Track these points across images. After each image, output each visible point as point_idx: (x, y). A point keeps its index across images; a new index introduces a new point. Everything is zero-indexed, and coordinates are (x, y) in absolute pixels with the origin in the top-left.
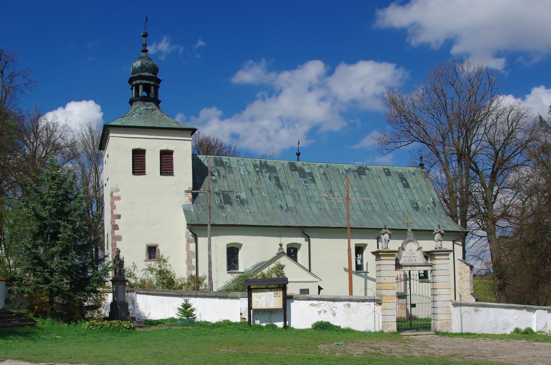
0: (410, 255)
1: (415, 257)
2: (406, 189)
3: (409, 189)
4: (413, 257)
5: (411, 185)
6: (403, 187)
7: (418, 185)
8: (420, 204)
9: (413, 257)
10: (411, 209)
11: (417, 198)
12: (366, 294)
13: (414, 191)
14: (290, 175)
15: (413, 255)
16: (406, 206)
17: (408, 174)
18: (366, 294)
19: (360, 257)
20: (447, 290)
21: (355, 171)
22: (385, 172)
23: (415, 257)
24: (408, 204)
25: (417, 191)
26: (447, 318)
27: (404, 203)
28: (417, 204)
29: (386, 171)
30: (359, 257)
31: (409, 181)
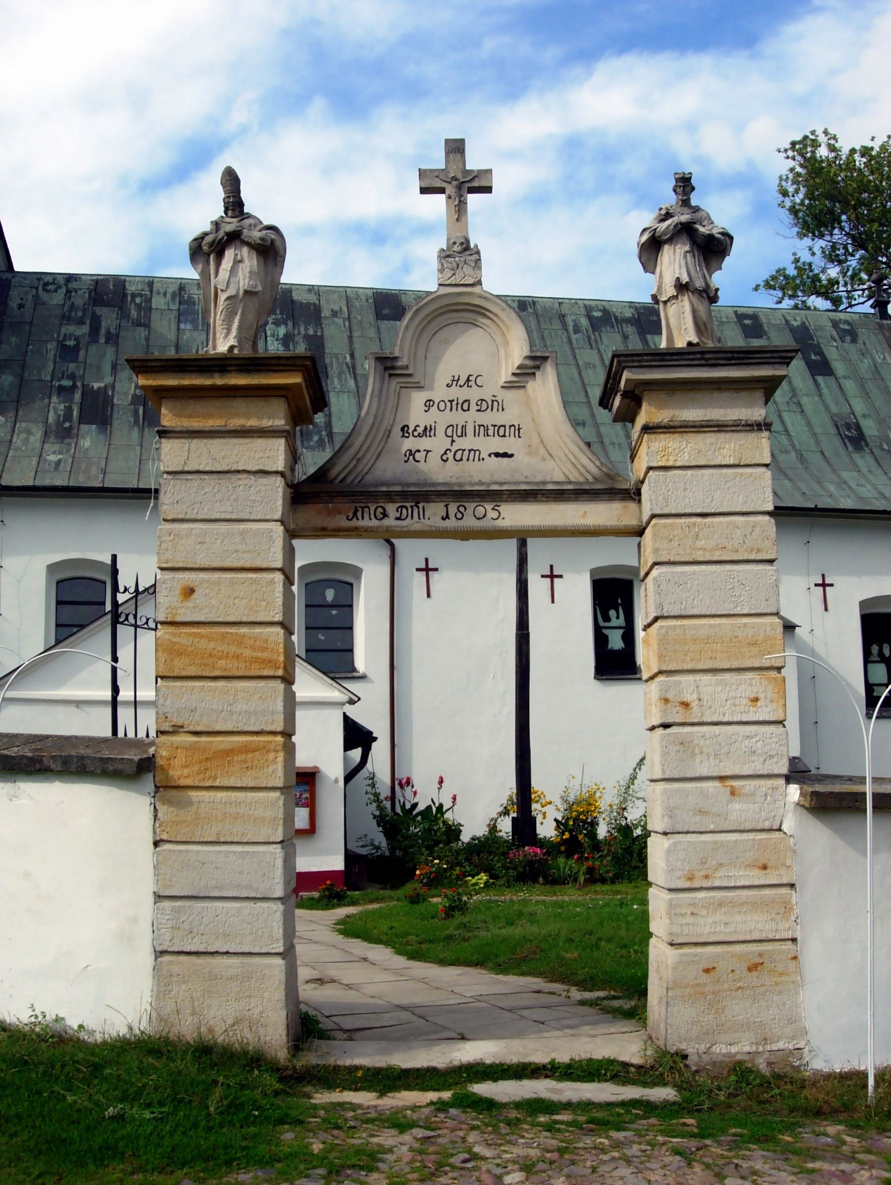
0: (458, 418)
1: (500, 430)
2: (820, 379)
3: (831, 380)
4: (483, 430)
5: (839, 367)
6: (807, 374)
7: (865, 365)
8: (870, 428)
9: (483, 430)
10: (833, 444)
11: (859, 406)
12: (136, 735)
13: (850, 386)
14: (372, 333)
15: (489, 418)
16: (815, 435)
17: (831, 331)
18: (136, 735)
19: (621, 621)
20: (751, 684)
21: (628, 321)
22: (744, 327)
23: (500, 430)
24: (822, 423)
25: (861, 383)
26: (757, 924)
27: (809, 423)
28: (858, 427)
29: (747, 322)
30: (617, 619)
31: (832, 353)
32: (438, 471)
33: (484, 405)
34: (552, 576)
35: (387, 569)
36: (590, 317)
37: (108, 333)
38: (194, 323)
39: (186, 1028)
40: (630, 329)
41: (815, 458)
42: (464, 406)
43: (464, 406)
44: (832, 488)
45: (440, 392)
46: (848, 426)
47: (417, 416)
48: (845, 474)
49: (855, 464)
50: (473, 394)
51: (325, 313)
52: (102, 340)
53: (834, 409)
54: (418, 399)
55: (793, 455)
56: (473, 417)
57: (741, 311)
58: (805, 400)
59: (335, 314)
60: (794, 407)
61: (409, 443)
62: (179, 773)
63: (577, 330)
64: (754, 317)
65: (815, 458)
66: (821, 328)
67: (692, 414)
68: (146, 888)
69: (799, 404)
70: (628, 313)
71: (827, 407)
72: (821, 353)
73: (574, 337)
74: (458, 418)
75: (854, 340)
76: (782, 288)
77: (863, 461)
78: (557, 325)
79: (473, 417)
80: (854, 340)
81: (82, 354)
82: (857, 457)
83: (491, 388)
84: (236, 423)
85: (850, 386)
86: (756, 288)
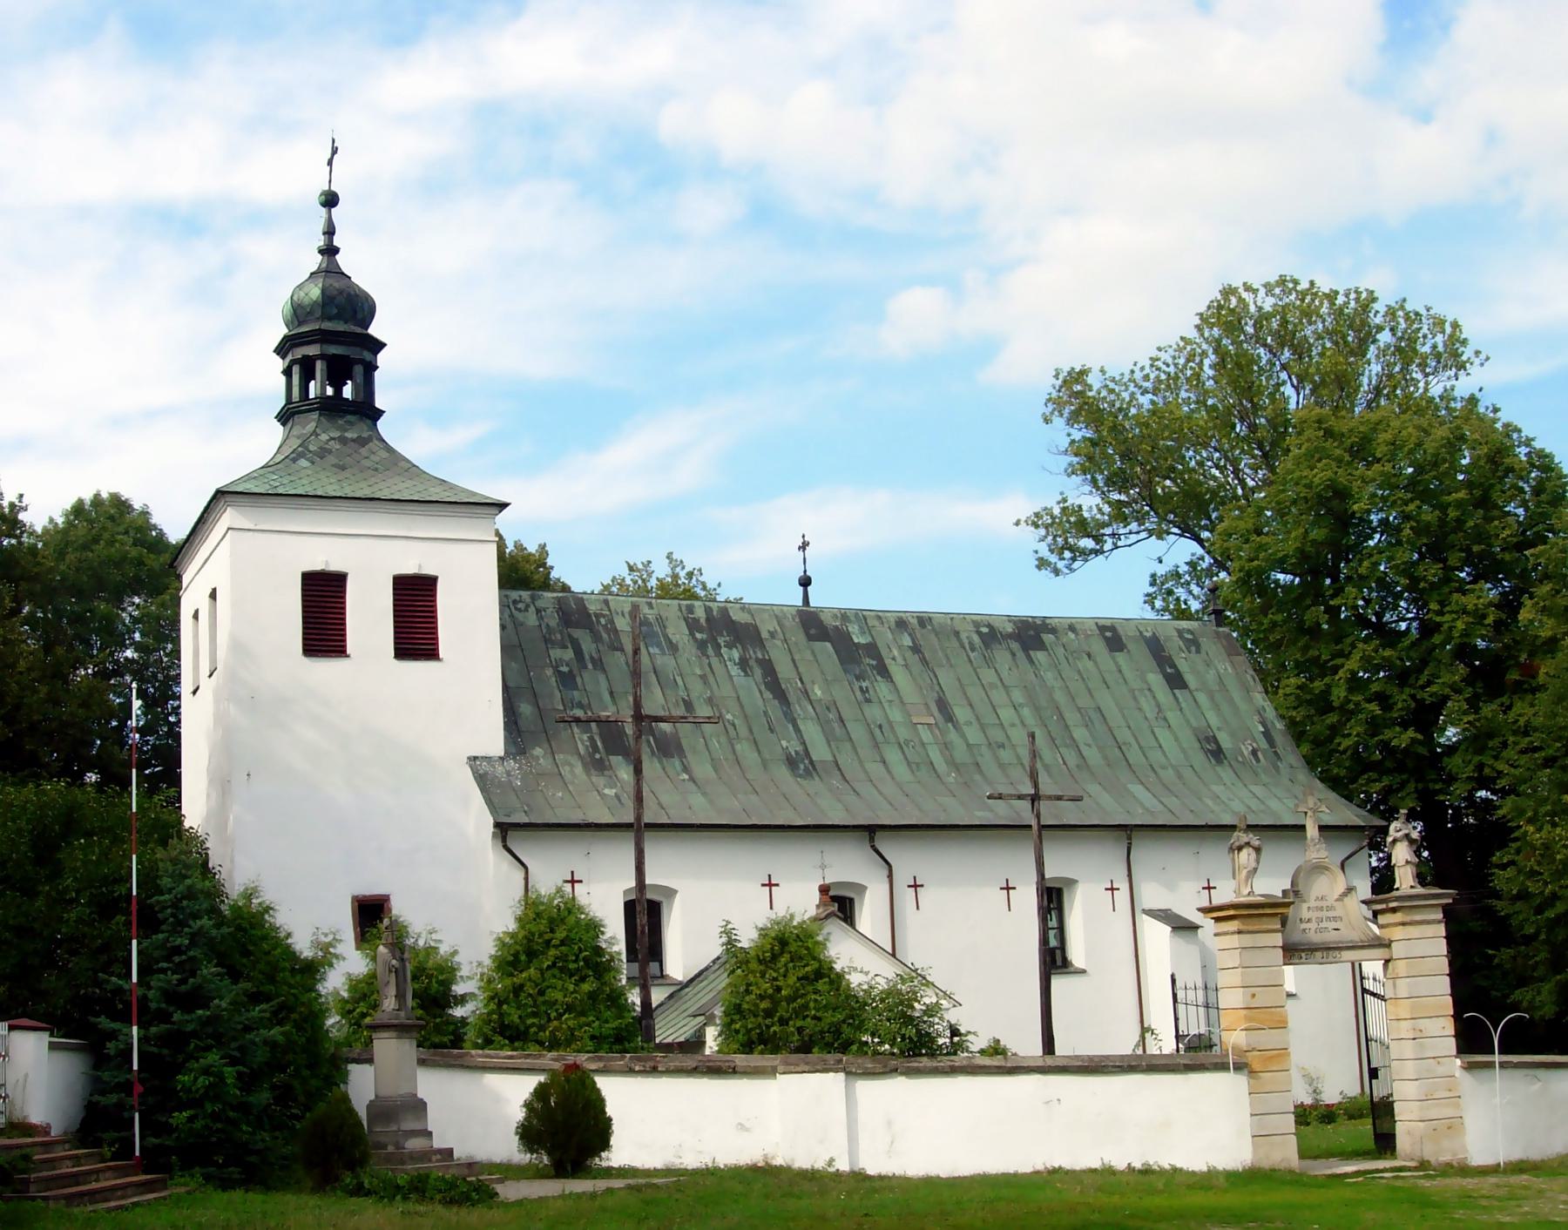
0: (1320, 914)
1: (1335, 919)
3: (1185, 692)
4: (1329, 919)
7: (1211, 676)
8: (1225, 741)
9: (1329, 919)
10: (1199, 759)
13: (1202, 698)
15: (1331, 914)
21: (1010, 636)
23: (1335, 919)
27: (1177, 739)
29: (1108, 634)
32: (1316, 938)
33: (1329, 908)
34: (1008, 889)
35: (887, 886)
36: (979, 633)
37: (592, 658)
38: (659, 645)
39: (1266, 1164)
40: (1015, 646)
41: (1187, 773)
42: (1321, 909)
43: (1321, 909)
44: (1210, 803)
45: (1312, 904)
46: (1207, 739)
47: (1305, 914)
48: (1214, 788)
49: (1220, 778)
50: (1324, 904)
51: (765, 635)
52: (590, 666)
53: (1195, 724)
54: (1305, 906)
55: (1170, 771)
56: (1325, 914)
57: (1101, 622)
58: (1169, 715)
59: (772, 635)
60: (1162, 723)
61: (1304, 926)
62: (1256, 1067)
63: (973, 650)
64: (1112, 629)
65: (1187, 773)
66: (1168, 638)
67: (1418, 917)
68: (1248, 1112)
69: (1165, 719)
70: (1009, 628)
71: (1188, 721)
72: (1173, 666)
73: (972, 655)
74: (1320, 914)
75: (1198, 651)
76: (1047, 527)
77: (1225, 773)
78: (955, 644)
79: (1325, 914)
80: (1198, 651)
81: (579, 680)
82: (1218, 769)
83: (1331, 901)
84: (1265, 927)
85: (1202, 698)
86: (1017, 523)
